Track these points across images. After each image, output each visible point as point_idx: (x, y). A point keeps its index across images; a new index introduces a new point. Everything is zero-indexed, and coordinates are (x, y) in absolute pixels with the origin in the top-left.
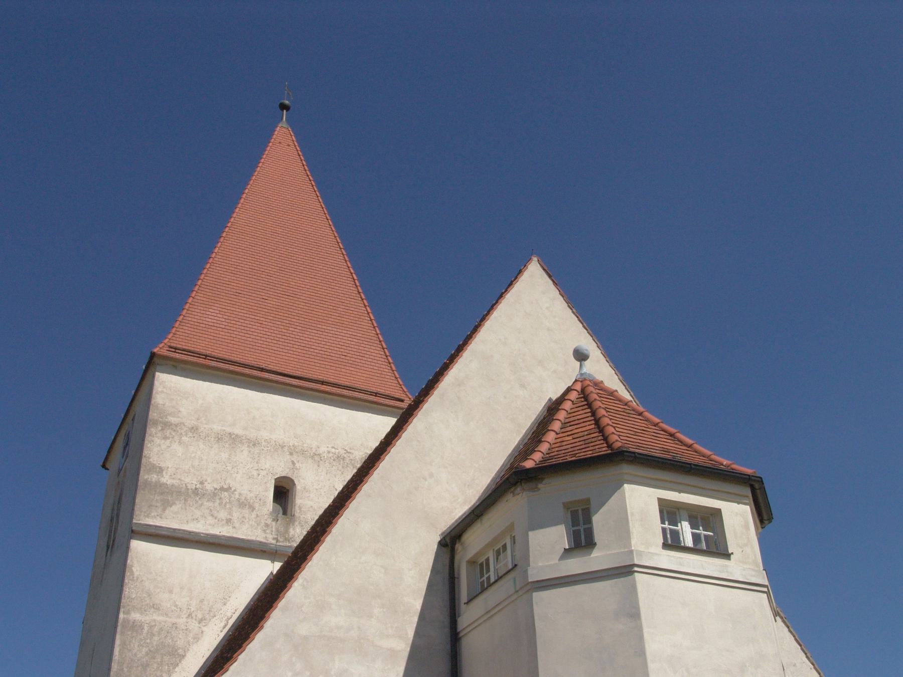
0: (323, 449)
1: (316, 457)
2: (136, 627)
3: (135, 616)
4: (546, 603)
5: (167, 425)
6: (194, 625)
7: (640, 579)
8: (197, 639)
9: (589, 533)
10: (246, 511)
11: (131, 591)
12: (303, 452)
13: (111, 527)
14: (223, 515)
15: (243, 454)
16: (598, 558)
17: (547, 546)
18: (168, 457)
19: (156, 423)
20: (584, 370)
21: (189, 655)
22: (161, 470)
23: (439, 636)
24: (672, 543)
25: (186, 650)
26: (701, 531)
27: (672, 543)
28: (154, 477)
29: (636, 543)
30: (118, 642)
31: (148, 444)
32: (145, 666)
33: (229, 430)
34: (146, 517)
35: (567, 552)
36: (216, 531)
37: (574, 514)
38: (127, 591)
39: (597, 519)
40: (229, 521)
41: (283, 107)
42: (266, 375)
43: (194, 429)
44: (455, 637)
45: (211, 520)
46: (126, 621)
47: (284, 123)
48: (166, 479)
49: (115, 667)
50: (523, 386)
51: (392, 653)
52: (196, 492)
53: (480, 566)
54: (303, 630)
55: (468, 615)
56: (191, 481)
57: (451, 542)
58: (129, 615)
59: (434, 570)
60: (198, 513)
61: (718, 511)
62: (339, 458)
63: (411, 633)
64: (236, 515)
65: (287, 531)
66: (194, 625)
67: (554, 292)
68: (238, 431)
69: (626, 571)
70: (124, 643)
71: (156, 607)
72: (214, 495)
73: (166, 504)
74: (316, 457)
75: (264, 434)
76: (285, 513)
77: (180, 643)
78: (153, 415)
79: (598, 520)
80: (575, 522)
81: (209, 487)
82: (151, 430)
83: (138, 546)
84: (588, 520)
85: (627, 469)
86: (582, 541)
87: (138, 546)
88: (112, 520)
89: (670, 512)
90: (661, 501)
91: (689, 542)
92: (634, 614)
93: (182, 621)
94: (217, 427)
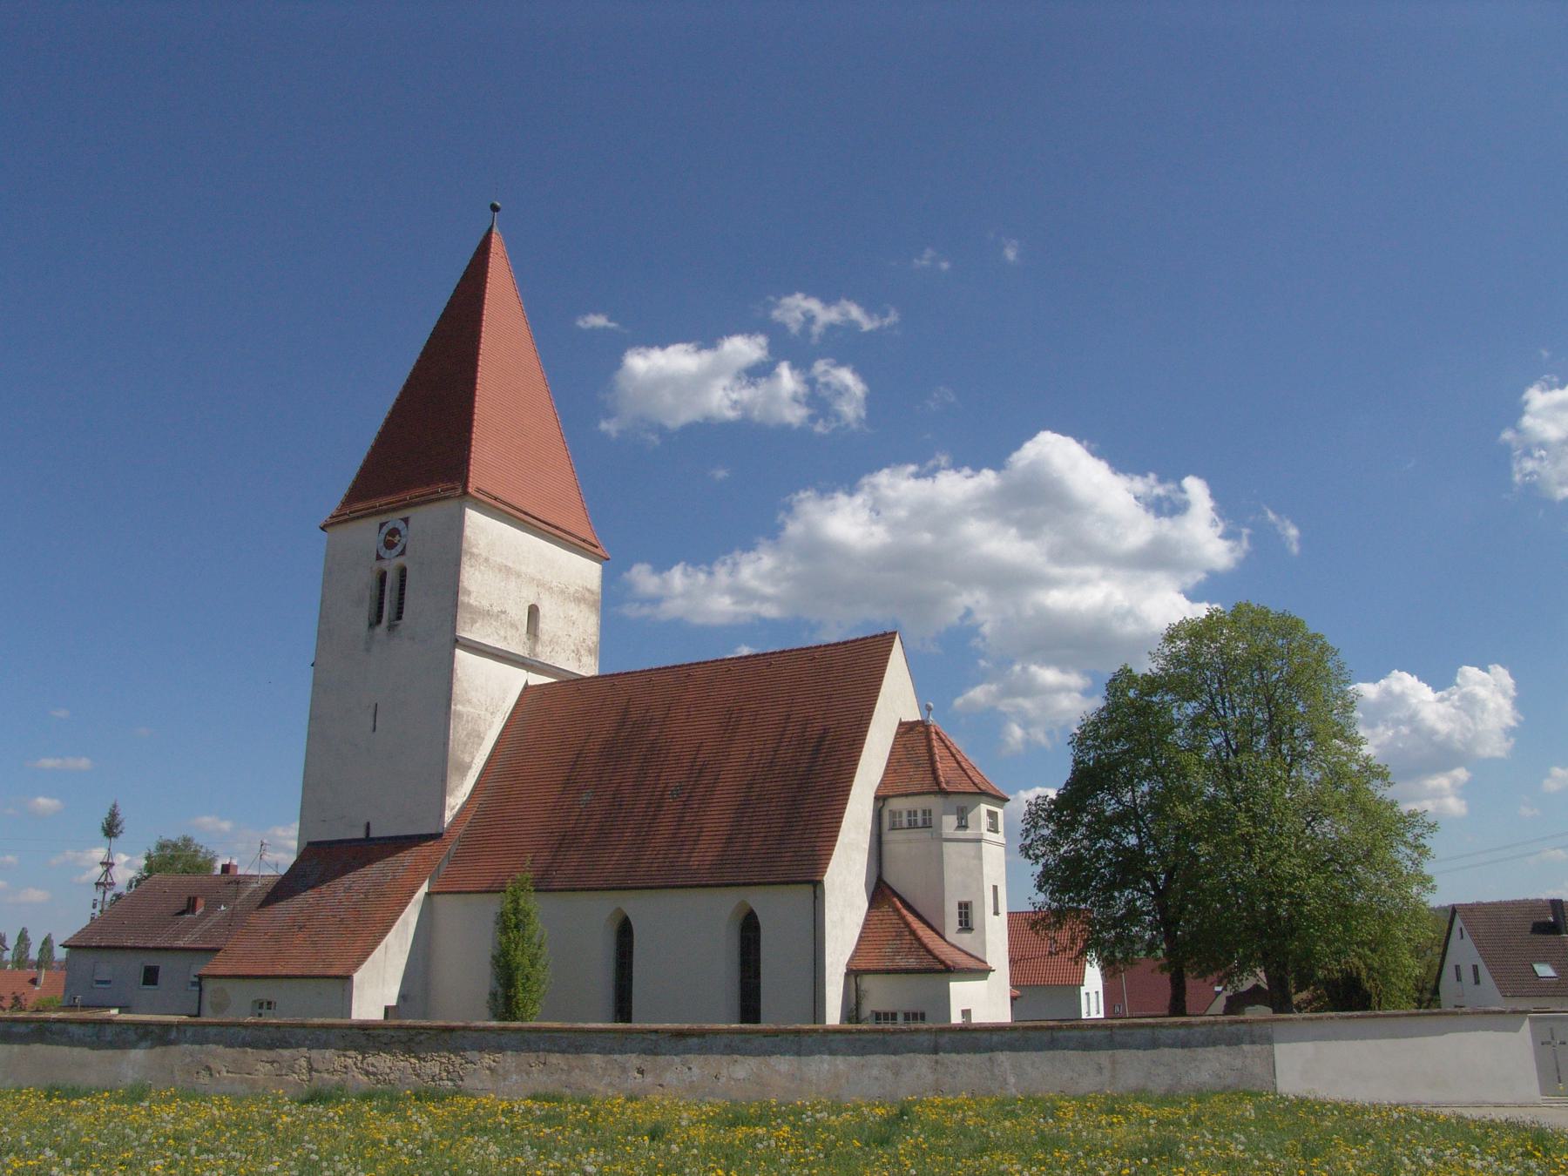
2: (460, 715)
3: (459, 707)
4: (948, 848)
5: (472, 554)
7: (984, 844)
11: (456, 689)
14: (502, 633)
16: (969, 833)
17: (949, 822)
18: (476, 583)
22: (469, 593)
34: (465, 632)
43: (487, 560)
53: (893, 813)
55: (889, 836)
56: (485, 604)
58: (457, 707)
62: (562, 592)
68: (510, 564)
69: (979, 841)
71: (469, 701)
73: (474, 622)
75: (524, 569)
77: (482, 729)
81: (496, 609)
82: (465, 559)
86: (962, 826)
87: (459, 653)
92: (980, 858)
94: (499, 560)
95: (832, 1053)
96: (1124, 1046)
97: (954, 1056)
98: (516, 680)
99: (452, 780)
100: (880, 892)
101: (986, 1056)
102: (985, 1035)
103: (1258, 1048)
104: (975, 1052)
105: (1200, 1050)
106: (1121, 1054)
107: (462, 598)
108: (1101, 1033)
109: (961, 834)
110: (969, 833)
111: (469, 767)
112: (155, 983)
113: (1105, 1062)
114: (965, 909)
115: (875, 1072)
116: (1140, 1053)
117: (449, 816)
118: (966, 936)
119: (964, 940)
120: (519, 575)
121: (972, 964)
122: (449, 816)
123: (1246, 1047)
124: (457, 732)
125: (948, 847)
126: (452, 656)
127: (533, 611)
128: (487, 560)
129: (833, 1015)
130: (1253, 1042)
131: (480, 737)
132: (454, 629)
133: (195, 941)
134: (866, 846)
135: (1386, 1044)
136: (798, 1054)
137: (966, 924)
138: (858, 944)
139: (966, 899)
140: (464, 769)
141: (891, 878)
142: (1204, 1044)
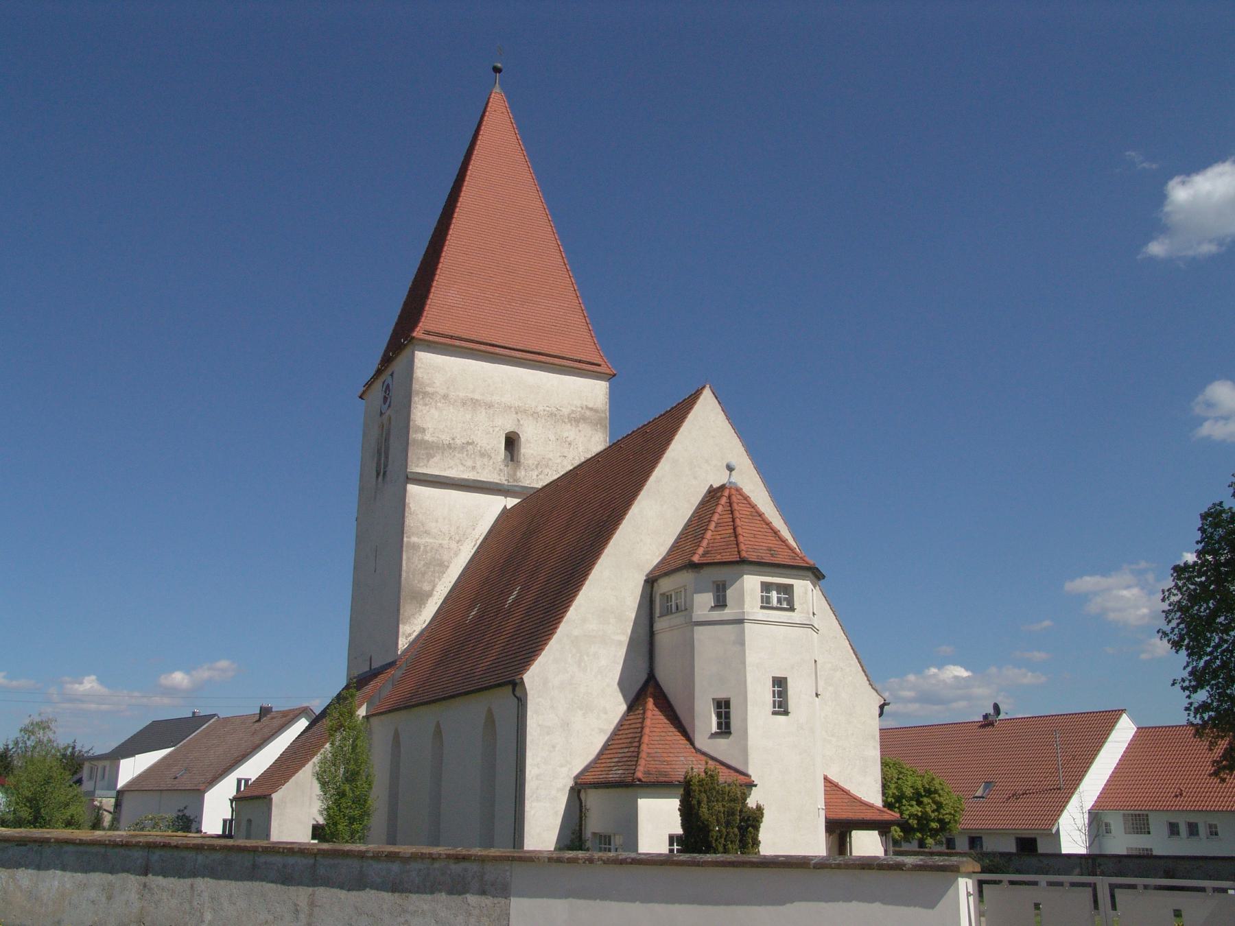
0: (540, 408)
1: (535, 415)
2: (415, 547)
3: (414, 539)
5: (426, 394)
6: (454, 545)
8: (456, 554)
9: (725, 600)
10: (485, 460)
11: (410, 522)
12: (525, 411)
13: (379, 459)
14: (469, 463)
15: (482, 415)
16: (727, 613)
17: (703, 602)
18: (430, 420)
19: (418, 393)
20: (733, 480)
21: (452, 566)
22: (424, 430)
23: (644, 631)
24: (766, 605)
25: (449, 562)
26: (783, 596)
27: (766, 605)
28: (419, 436)
29: (747, 608)
30: (404, 557)
31: (413, 410)
32: (424, 574)
33: (471, 396)
34: (418, 467)
35: (713, 608)
36: (465, 476)
37: (718, 586)
38: (407, 522)
39: (729, 592)
40: (474, 468)
41: (497, 70)
42: (498, 350)
43: (445, 397)
44: (652, 634)
45: (461, 468)
46: (409, 543)
47: (497, 89)
48: (428, 437)
49: (404, 575)
50: (695, 478)
51: (620, 642)
52: (449, 446)
53: (667, 597)
54: (576, 632)
55: (660, 624)
56: (446, 438)
57: (651, 582)
58: (411, 539)
59: (642, 596)
60: (452, 463)
61: (791, 586)
62: (552, 415)
63: (629, 632)
64: (478, 464)
65: (515, 474)
66: (454, 545)
67: (722, 416)
68: (477, 397)
69: (740, 621)
70: (408, 558)
71: (427, 533)
72: (463, 448)
73: (430, 457)
74: (535, 415)
75: (496, 398)
76: (512, 460)
77: (445, 558)
78: (415, 386)
79: (730, 593)
80: (718, 590)
81: (458, 442)
82: (415, 399)
83: (412, 489)
84: (724, 590)
85: (746, 567)
86: (721, 603)
87: (412, 489)
88: (379, 452)
89: (766, 587)
90: (763, 584)
91: (775, 602)
92: (742, 644)
93: (445, 542)
94: (462, 395)
95: (64, 869)
96: (328, 883)
97: (160, 880)
98: (492, 508)
99: (406, 609)
100: (650, 688)
101: (189, 881)
102: (191, 855)
103: (487, 901)
104: (181, 876)
105: (414, 897)
106: (322, 893)
107: (414, 436)
108: (303, 861)
109: (717, 615)
110: (727, 613)
111: (429, 594)
113: (303, 903)
114: (723, 707)
115: (92, 894)
116: (342, 894)
117: (403, 644)
118: (722, 742)
119: (721, 748)
122: (403, 644)
123: (472, 899)
124: (411, 564)
126: (405, 490)
127: (511, 442)
129: (542, 827)
130: (483, 893)
131: (443, 566)
133: (610, 769)
134: (625, 639)
136: (38, 868)
137: (725, 728)
138: (601, 753)
139: (722, 695)
140: (421, 598)
141: (662, 675)
142: (419, 890)
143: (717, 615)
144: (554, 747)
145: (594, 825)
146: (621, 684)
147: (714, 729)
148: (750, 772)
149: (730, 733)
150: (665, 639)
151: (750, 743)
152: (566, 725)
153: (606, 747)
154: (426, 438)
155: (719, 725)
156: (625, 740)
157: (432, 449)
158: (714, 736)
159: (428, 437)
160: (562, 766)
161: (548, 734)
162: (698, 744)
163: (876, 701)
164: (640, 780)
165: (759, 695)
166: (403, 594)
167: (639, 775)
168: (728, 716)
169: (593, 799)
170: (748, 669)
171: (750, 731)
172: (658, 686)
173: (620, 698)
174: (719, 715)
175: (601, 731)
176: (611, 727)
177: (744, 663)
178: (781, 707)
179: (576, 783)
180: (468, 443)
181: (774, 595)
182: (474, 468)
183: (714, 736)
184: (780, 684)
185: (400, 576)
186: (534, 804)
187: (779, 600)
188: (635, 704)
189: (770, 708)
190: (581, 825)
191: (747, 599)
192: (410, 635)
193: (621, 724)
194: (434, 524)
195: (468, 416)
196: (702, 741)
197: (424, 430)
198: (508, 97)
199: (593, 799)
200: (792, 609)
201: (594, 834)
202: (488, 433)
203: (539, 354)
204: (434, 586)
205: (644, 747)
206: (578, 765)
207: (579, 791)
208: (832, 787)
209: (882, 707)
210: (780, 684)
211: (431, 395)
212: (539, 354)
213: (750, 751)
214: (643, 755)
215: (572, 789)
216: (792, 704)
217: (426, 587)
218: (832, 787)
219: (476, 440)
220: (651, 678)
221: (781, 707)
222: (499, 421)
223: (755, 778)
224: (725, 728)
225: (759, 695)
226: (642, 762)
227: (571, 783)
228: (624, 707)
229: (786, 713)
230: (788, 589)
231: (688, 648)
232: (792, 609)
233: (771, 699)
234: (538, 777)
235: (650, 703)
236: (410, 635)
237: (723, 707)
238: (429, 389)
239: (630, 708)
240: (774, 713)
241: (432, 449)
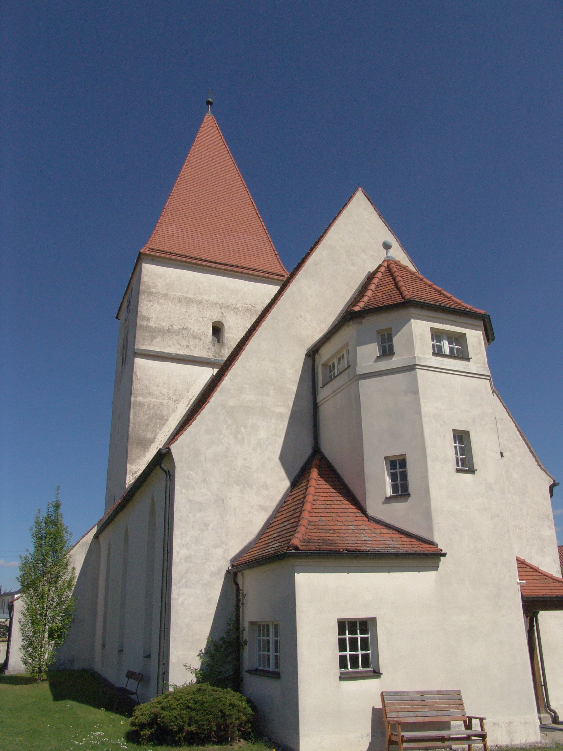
0: (239, 305)
1: (235, 310)
2: (141, 405)
3: (140, 399)
5: (150, 293)
6: (172, 404)
8: (174, 410)
10: (197, 341)
11: (137, 385)
12: (228, 307)
14: (184, 343)
15: (194, 309)
16: (395, 362)
17: (367, 355)
18: (151, 311)
19: (144, 293)
21: (170, 419)
22: (148, 319)
23: (307, 405)
26: (454, 346)
27: (438, 352)
28: (145, 323)
30: (132, 413)
32: (147, 425)
33: (185, 295)
35: (379, 358)
36: (181, 352)
39: (395, 339)
41: (209, 103)
42: (205, 263)
43: (166, 296)
44: (315, 406)
45: (178, 347)
46: (135, 401)
49: (131, 425)
50: (353, 265)
51: (281, 415)
52: (168, 331)
54: (232, 403)
55: (322, 394)
56: (166, 325)
59: (304, 370)
60: (170, 342)
63: (291, 404)
64: (192, 343)
65: (220, 351)
67: (371, 209)
68: (190, 296)
69: (411, 368)
70: (135, 414)
71: (151, 394)
72: (179, 332)
73: (153, 338)
74: (235, 310)
75: (205, 297)
76: (219, 341)
77: (165, 413)
78: (142, 288)
79: (397, 340)
80: (383, 341)
81: (176, 327)
82: (142, 297)
83: (138, 361)
84: (390, 340)
85: (413, 311)
86: (387, 351)
87: (138, 361)
89: (437, 335)
93: (165, 401)
94: (179, 294)
99: (133, 452)
107: (140, 322)
109: (383, 365)
110: (395, 362)
111: (152, 441)
112: (344, 626)
114: (398, 467)
118: (399, 506)
119: (399, 514)
120: (200, 302)
121: (426, 548)
124: (137, 418)
125: (363, 384)
128: (166, 296)
131: (163, 420)
132: (134, 346)
134: (286, 411)
135: (180, 419)
137: (401, 490)
139: (395, 452)
140: (145, 444)
143: (383, 365)
144: (206, 525)
145: (251, 613)
146: (283, 458)
147: (389, 492)
148: (436, 539)
149: (409, 495)
150: (328, 409)
151: (433, 505)
152: (220, 501)
153: (268, 525)
154: (150, 324)
155: (395, 488)
156: (288, 513)
157: (155, 332)
158: (388, 500)
159: (152, 324)
160: (216, 546)
161: (200, 510)
162: (370, 512)
163: (547, 482)
164: (296, 548)
165: (440, 452)
166: (130, 440)
167: (296, 541)
168: (404, 476)
169: (250, 581)
170: (425, 420)
171: (433, 492)
172: (323, 458)
173: (283, 473)
174: (393, 477)
175: (262, 508)
176: (273, 505)
177: (419, 413)
178: (466, 465)
179: (233, 566)
180: (183, 329)
181: (446, 346)
182: (188, 347)
183: (388, 500)
184: (462, 438)
185: (129, 426)
186: (182, 590)
187: (451, 349)
188: (298, 480)
189: (452, 466)
190: (238, 615)
191: (417, 344)
192: (136, 472)
193: (284, 502)
194: (156, 388)
195: (183, 310)
196: (374, 507)
197: (148, 319)
198: (215, 117)
199: (250, 581)
200: (376, 674)
201: (252, 623)
202: (199, 322)
203: (237, 267)
204: (156, 435)
205: (305, 515)
206: (236, 547)
207: (235, 574)
208: (523, 566)
209: (551, 488)
210: (462, 438)
211: (155, 294)
212: (237, 267)
213: (434, 514)
214: (304, 522)
215: (228, 572)
216: (477, 461)
217: (150, 435)
218: (523, 566)
219: (190, 326)
220: (317, 451)
221: (466, 465)
222: (208, 314)
223: (442, 546)
224: (401, 490)
225: (440, 452)
226: (301, 530)
227: (226, 566)
228: (286, 484)
229: (472, 471)
230: (460, 339)
231: (355, 404)
232: (376, 674)
233: (454, 456)
234: (187, 559)
235: (314, 473)
236: (136, 472)
237: (398, 467)
238: (154, 290)
239: (294, 484)
240: (458, 471)
241: (155, 332)
